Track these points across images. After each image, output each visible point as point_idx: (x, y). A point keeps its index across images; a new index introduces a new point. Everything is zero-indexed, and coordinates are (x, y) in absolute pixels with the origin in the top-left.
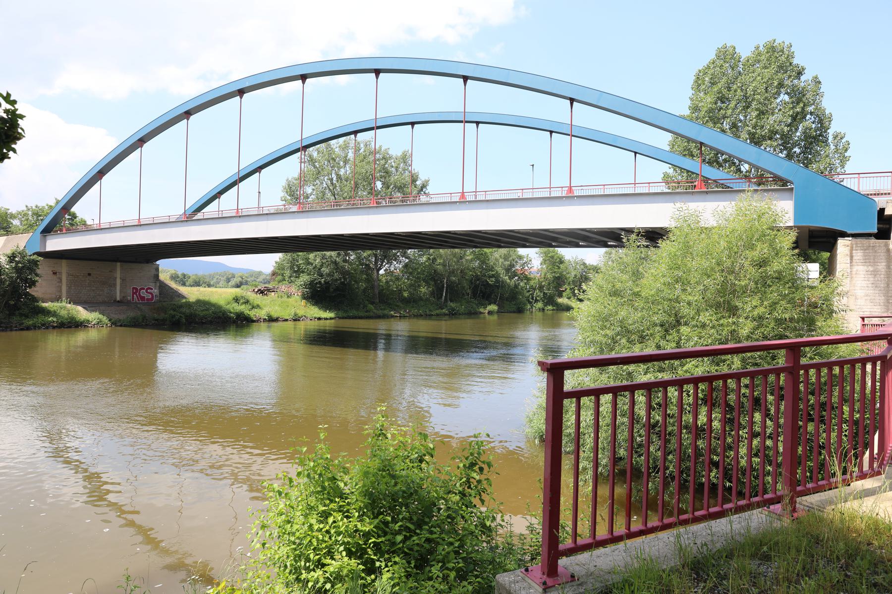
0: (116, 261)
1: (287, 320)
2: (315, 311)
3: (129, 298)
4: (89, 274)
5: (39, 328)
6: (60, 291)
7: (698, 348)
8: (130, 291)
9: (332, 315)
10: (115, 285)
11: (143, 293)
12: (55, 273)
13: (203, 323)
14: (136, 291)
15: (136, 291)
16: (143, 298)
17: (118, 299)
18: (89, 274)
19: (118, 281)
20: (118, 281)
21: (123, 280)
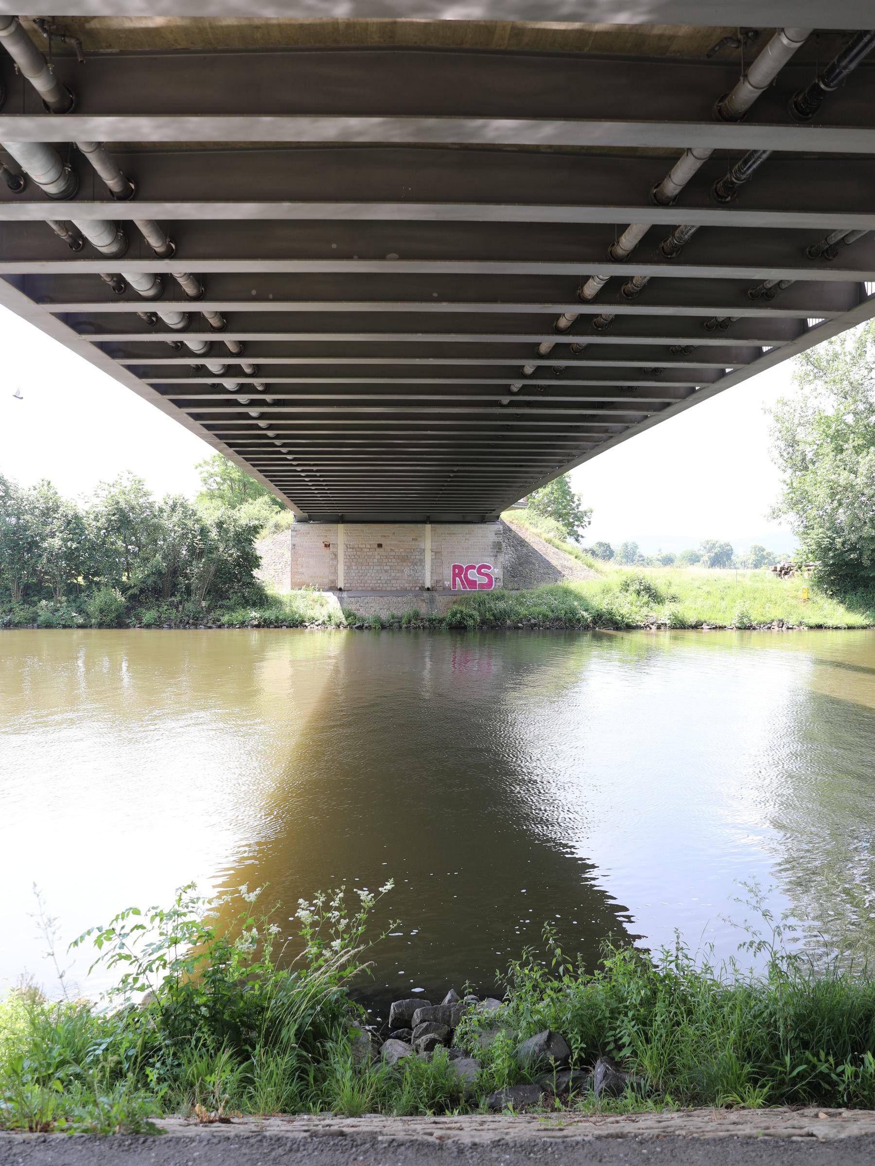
0: (424, 522)
1: (722, 628)
2: (836, 613)
3: (447, 583)
4: (380, 546)
5: (55, 627)
6: (336, 572)
7: (448, 525)
8: (448, 572)
9: (857, 618)
10: (422, 561)
11: (473, 575)
12: (327, 546)
13: (519, 628)
14: (458, 571)
15: (458, 571)
16: (472, 584)
17: (428, 584)
18: (380, 546)
19: (428, 557)
20: (428, 557)
21: (437, 553)
